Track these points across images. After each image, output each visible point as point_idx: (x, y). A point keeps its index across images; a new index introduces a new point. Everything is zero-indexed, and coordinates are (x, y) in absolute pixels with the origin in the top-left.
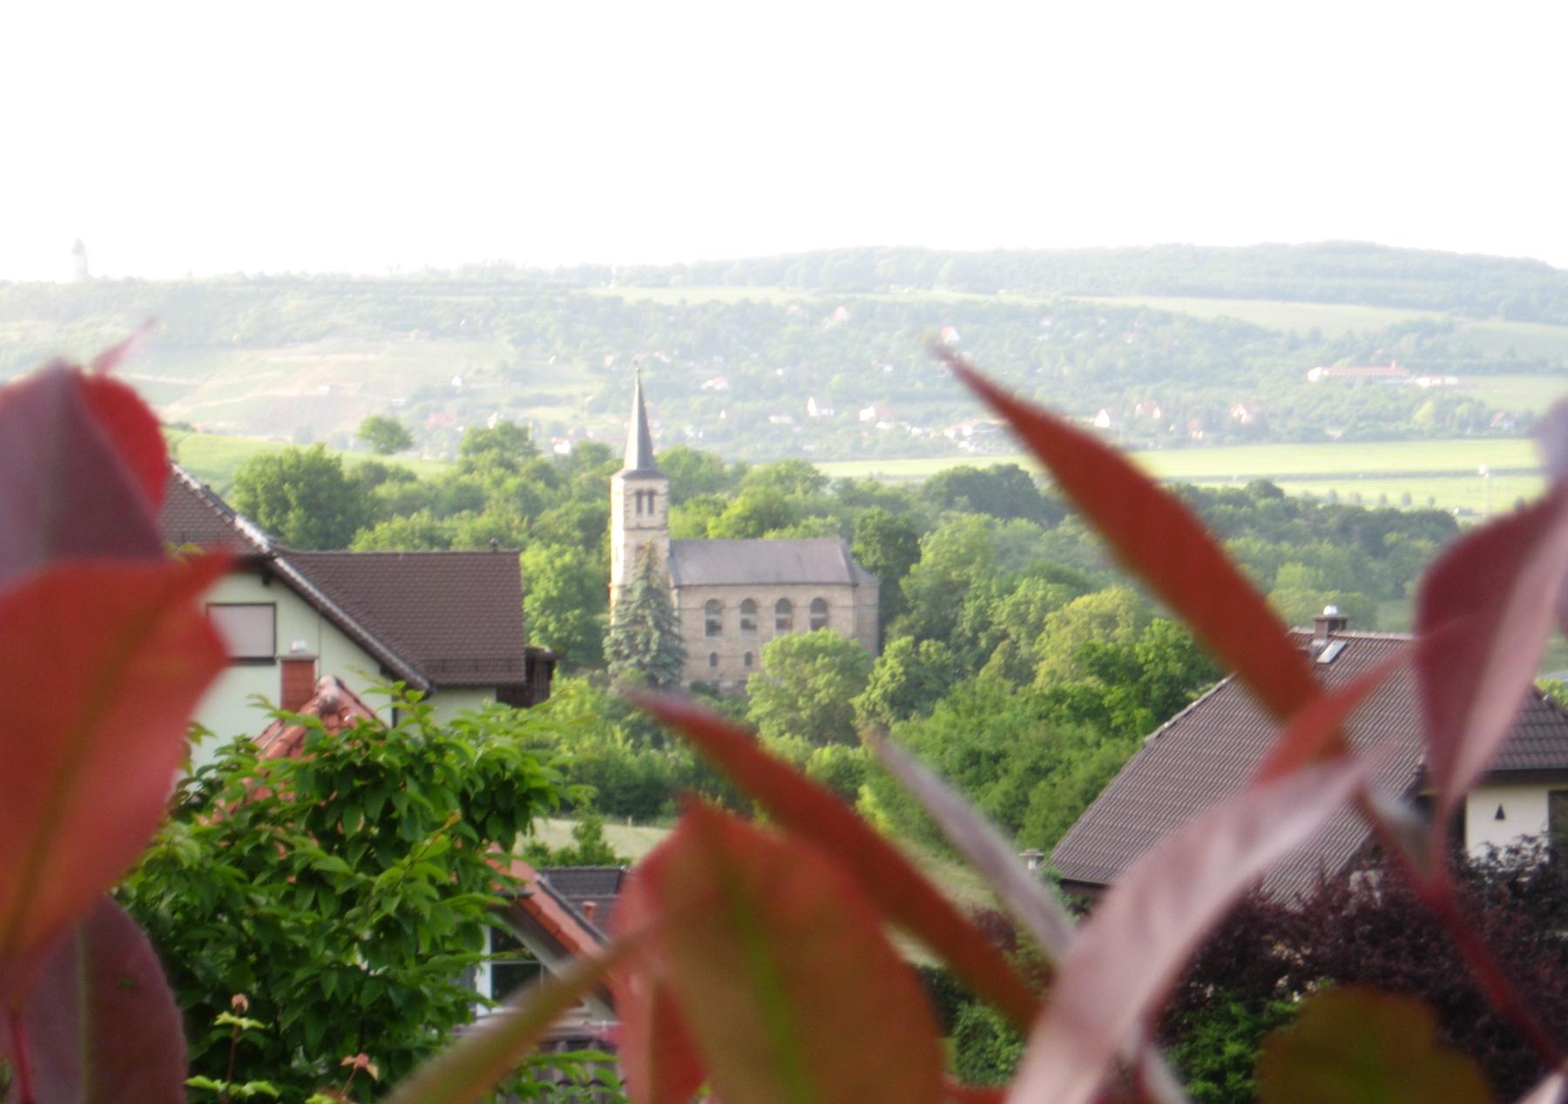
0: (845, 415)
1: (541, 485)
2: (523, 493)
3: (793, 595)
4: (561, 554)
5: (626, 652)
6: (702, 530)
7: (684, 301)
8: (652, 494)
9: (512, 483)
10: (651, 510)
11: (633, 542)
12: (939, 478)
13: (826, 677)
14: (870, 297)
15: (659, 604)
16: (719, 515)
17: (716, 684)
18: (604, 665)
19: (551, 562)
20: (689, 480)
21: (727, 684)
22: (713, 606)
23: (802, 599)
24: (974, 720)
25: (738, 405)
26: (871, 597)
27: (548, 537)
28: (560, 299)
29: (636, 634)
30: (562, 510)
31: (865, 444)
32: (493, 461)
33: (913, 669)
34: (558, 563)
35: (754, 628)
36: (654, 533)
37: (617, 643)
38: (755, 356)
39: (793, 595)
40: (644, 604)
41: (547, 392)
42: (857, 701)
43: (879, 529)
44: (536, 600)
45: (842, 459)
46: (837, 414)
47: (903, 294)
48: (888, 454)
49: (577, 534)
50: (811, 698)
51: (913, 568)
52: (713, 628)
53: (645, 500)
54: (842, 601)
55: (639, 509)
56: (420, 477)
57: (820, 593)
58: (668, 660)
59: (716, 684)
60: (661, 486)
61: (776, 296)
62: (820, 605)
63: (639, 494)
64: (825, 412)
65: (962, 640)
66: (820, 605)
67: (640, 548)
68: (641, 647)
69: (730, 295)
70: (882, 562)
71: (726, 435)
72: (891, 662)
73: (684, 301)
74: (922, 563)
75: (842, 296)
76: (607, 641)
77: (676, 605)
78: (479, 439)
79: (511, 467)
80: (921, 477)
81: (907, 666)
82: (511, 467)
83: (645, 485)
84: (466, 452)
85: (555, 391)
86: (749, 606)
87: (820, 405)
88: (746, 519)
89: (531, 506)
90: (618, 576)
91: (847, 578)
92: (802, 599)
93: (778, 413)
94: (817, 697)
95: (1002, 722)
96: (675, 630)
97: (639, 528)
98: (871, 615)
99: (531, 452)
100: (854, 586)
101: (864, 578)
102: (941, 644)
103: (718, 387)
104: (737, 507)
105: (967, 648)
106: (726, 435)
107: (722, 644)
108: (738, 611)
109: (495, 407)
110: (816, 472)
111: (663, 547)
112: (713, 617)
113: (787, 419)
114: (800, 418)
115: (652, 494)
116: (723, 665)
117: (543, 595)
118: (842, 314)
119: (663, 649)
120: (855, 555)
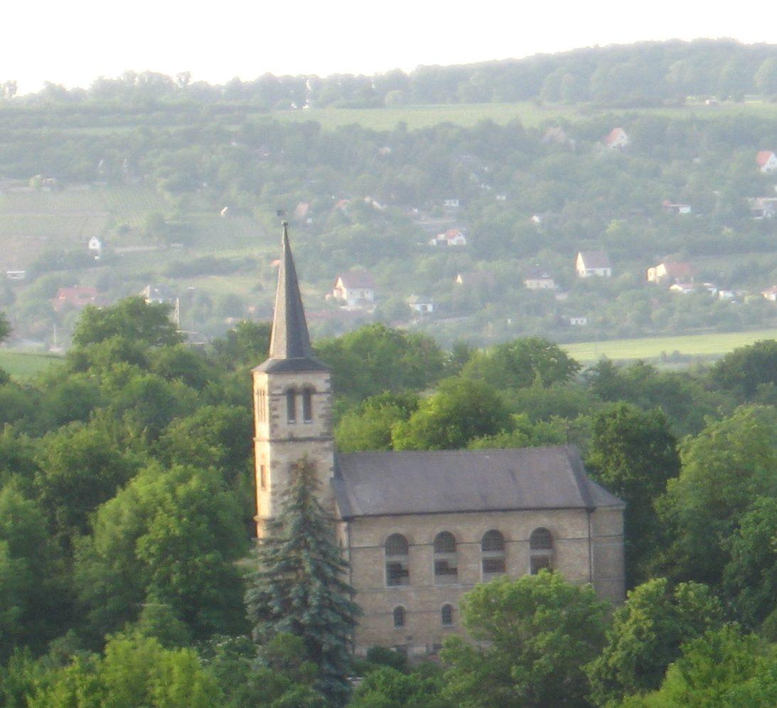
0: (627, 275)
1: (179, 384)
2: (152, 393)
3: (504, 524)
4: (184, 479)
5: (276, 609)
6: (384, 439)
7: (403, 126)
8: (308, 392)
9: (139, 380)
10: (308, 415)
11: (284, 459)
12: (736, 357)
13: (550, 636)
14: (659, 112)
15: (319, 543)
16: (407, 417)
17: (403, 650)
18: (246, 628)
19: (172, 490)
20: (369, 372)
21: (419, 650)
22: (399, 544)
23: (519, 530)
24: (712, 691)
25: (481, 265)
26: (612, 523)
27: (164, 455)
28: (233, 128)
29: (289, 584)
30: (198, 418)
31: (656, 313)
32: (114, 352)
33: (667, 622)
34: (181, 490)
35: (454, 571)
36: (313, 445)
37: (264, 598)
38: (502, 198)
39: (504, 524)
40: (298, 544)
41: (220, 255)
42: (592, 668)
43: (622, 431)
44: (151, 542)
45: (624, 335)
46: (615, 274)
47: (704, 106)
48: (683, 329)
49: (216, 451)
50: (529, 665)
51: (672, 484)
52: (398, 573)
53: (299, 400)
54: (572, 530)
55: (292, 414)
56: (15, 377)
57: (544, 521)
58: (334, 618)
59: (403, 650)
60: (321, 382)
61: (528, 115)
62: (543, 538)
63: (291, 393)
64: (600, 272)
65: (738, 580)
66: (543, 538)
67: (293, 467)
68: (295, 603)
69: (467, 116)
70: (628, 477)
71: (465, 307)
72: (636, 613)
73: (403, 126)
74: (683, 477)
75: (620, 113)
76: (250, 595)
77: (345, 544)
78: (101, 323)
79: (139, 361)
80: (713, 357)
81: (657, 618)
82: (139, 361)
83: (299, 380)
84: (83, 340)
85: (231, 254)
86: (447, 542)
87: (590, 263)
88: (445, 422)
89: (158, 410)
90: (265, 506)
91: (580, 502)
92: (519, 530)
93: (537, 275)
94: (537, 664)
95: (747, 694)
96: (346, 579)
97: (293, 439)
98: (614, 551)
99: (172, 338)
100: (590, 510)
101: (604, 499)
102: (703, 587)
103: (453, 242)
104: (432, 401)
105: (744, 592)
106: (465, 307)
107: (409, 596)
108: (432, 548)
109: (147, 278)
110: (562, 355)
111: (326, 461)
112: (396, 559)
113: (546, 284)
114: (567, 281)
115: (308, 392)
116: (411, 621)
117: (162, 534)
118: (620, 138)
119: (327, 604)
120: (591, 469)
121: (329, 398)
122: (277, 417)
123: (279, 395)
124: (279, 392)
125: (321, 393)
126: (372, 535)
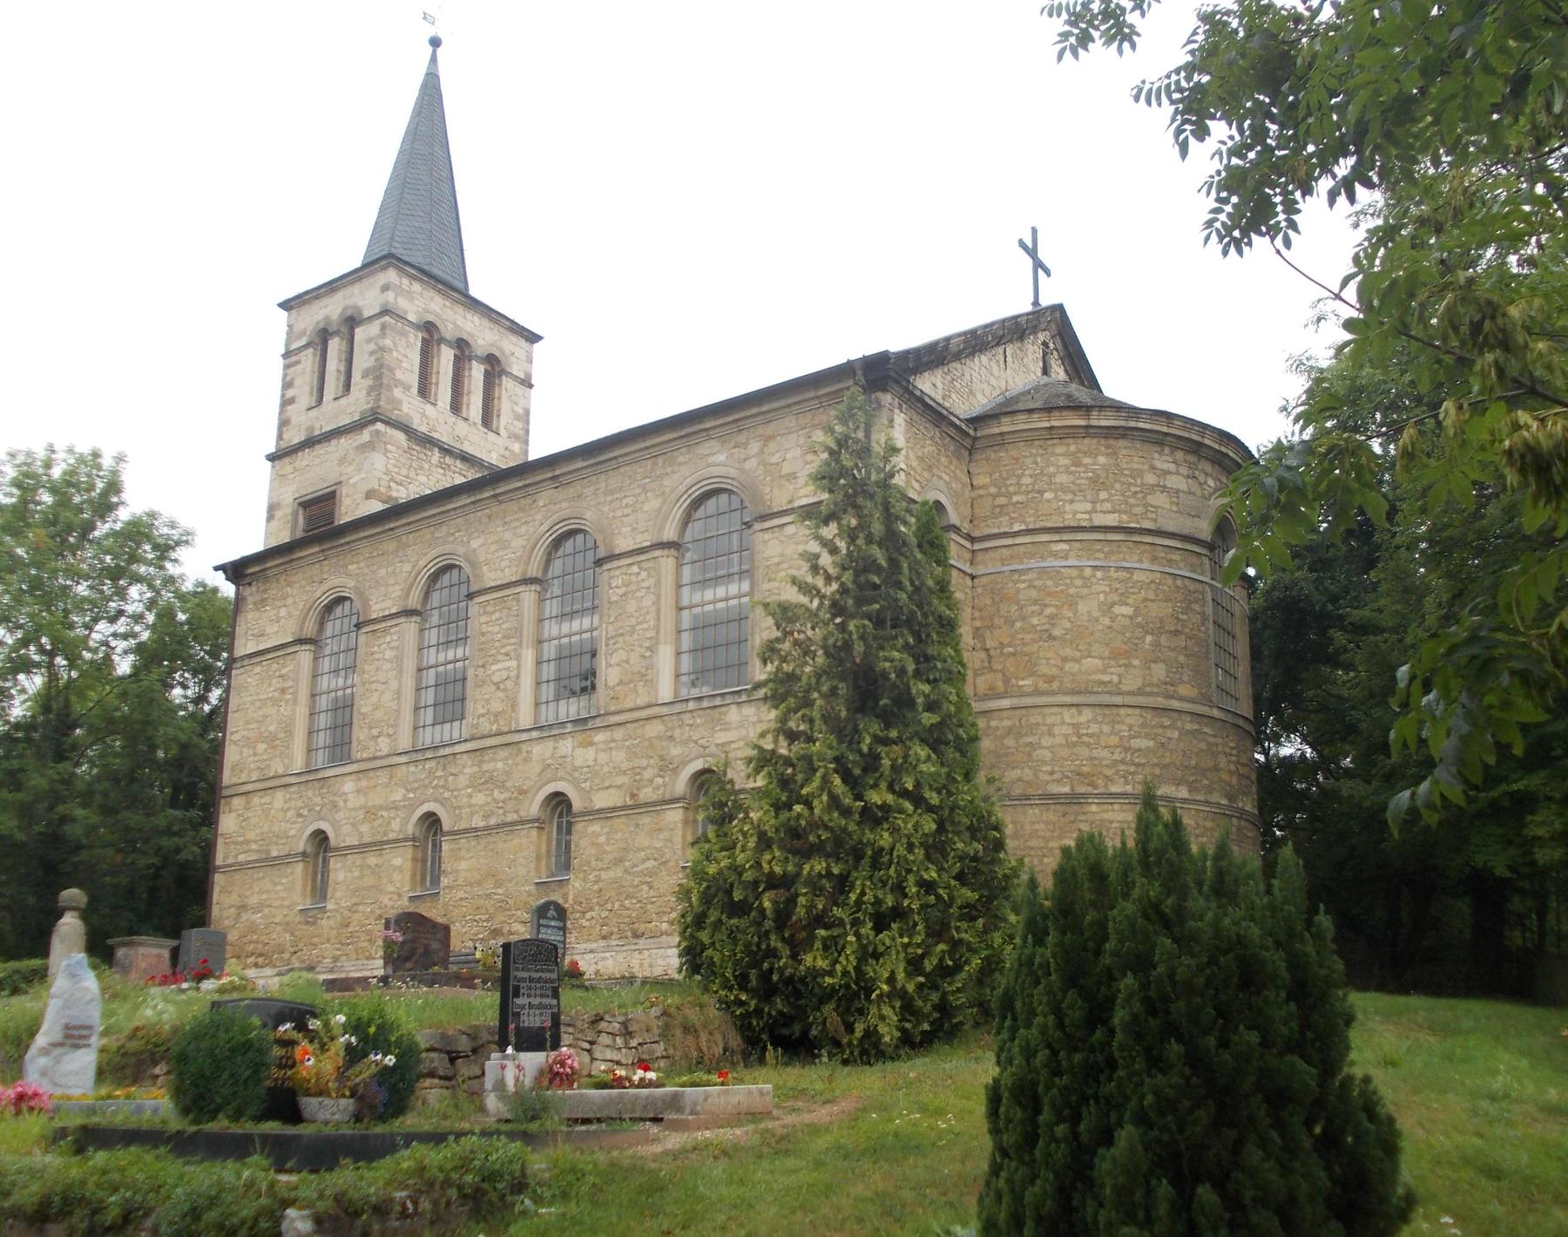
11: (289, 495)
121: (383, 327)
122: (291, 401)
123: (301, 349)
124: (303, 342)
125: (370, 319)
126: (283, 612)
